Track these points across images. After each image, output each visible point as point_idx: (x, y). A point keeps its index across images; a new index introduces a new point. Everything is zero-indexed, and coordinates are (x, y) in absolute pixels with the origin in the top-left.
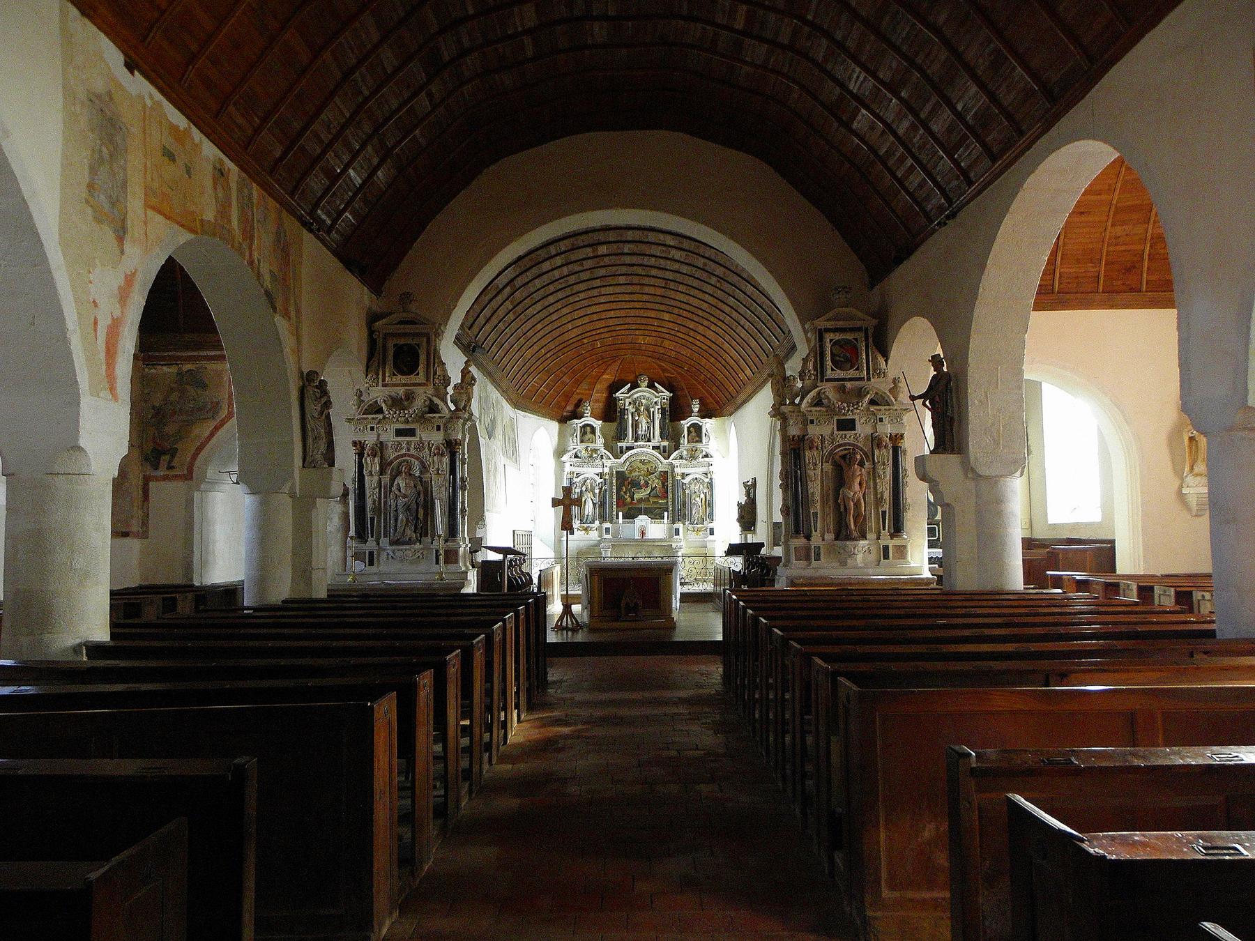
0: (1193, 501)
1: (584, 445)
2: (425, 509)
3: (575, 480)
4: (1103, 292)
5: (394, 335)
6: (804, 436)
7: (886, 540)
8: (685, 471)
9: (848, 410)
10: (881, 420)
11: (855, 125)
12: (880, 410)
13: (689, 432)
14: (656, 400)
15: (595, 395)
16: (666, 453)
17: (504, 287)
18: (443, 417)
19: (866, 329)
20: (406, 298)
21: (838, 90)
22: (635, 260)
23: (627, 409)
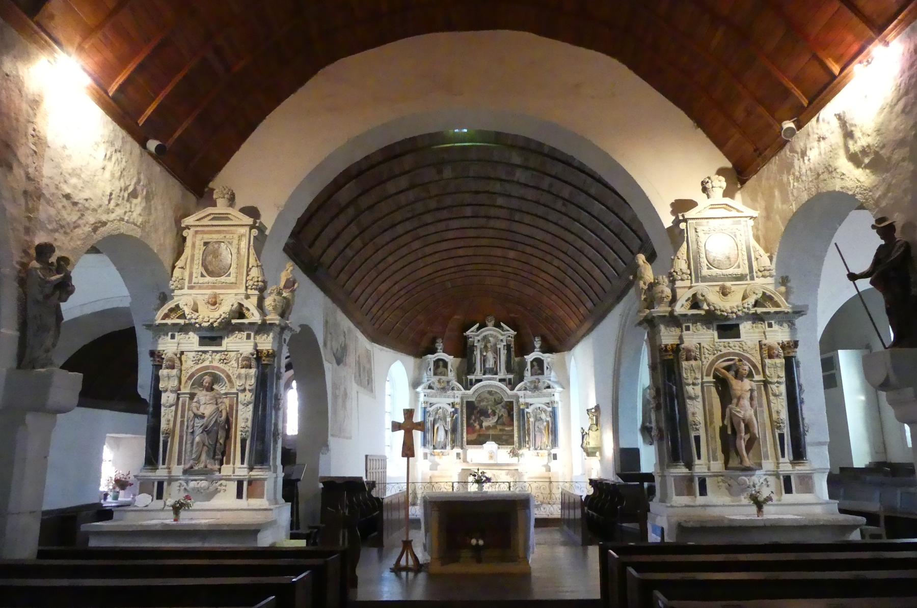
1: (437, 378)
3: (428, 409)
8: (529, 400)
13: (532, 366)
14: (501, 337)
15: (447, 334)
16: (512, 385)
17: (347, 206)
23: (476, 346)
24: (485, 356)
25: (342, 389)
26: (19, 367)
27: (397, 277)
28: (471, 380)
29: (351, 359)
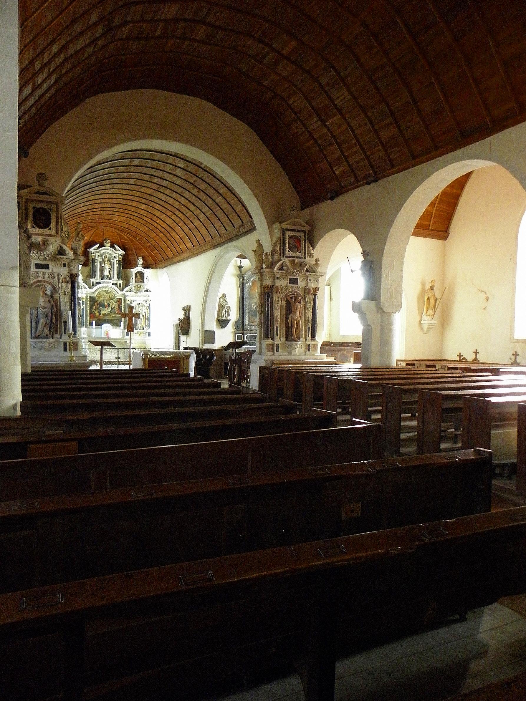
0: (425, 327)
2: (56, 316)
4: (431, 230)
5: (32, 201)
6: (273, 286)
7: (309, 342)
8: (133, 299)
9: (297, 274)
10: (310, 280)
11: (327, 123)
12: (310, 275)
13: (136, 276)
14: (115, 255)
16: (121, 288)
18: (69, 258)
19: (305, 231)
20: (41, 177)
21: (328, 101)
22: (151, 171)
23: (97, 259)
24: (103, 267)
28: (93, 283)
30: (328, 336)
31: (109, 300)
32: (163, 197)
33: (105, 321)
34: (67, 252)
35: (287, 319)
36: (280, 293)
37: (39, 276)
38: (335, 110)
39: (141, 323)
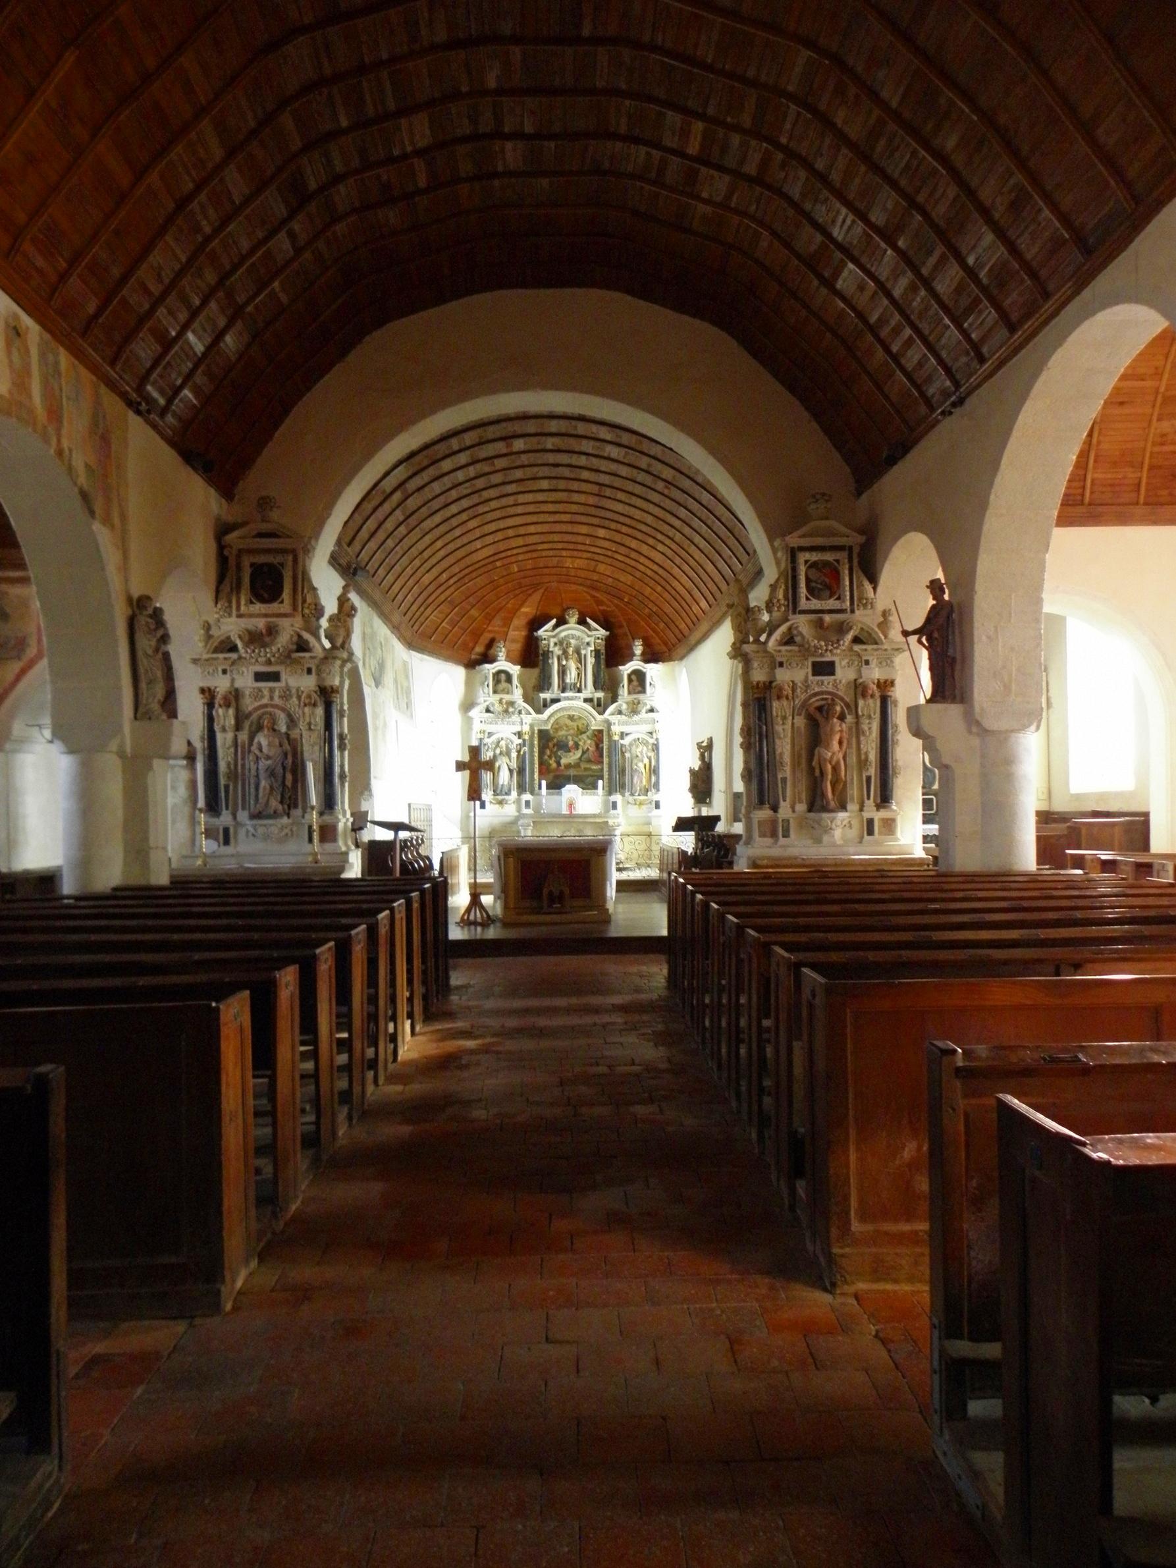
1: (498, 697)
4: (1146, 504)
5: (250, 551)
6: (771, 682)
7: (870, 812)
8: (625, 729)
9: (826, 650)
10: (867, 663)
13: (630, 681)
14: (588, 640)
16: (600, 707)
21: (819, 238)
23: (552, 652)
25: (381, 717)
26: (136, 718)
27: (445, 564)
28: (545, 700)
29: (388, 678)
30: (1045, 796)
31: (577, 736)
32: (620, 507)
33: (568, 780)
34: (311, 645)
35: (811, 758)
36: (787, 698)
37: (262, 697)
38: (838, 255)
39: (641, 782)
